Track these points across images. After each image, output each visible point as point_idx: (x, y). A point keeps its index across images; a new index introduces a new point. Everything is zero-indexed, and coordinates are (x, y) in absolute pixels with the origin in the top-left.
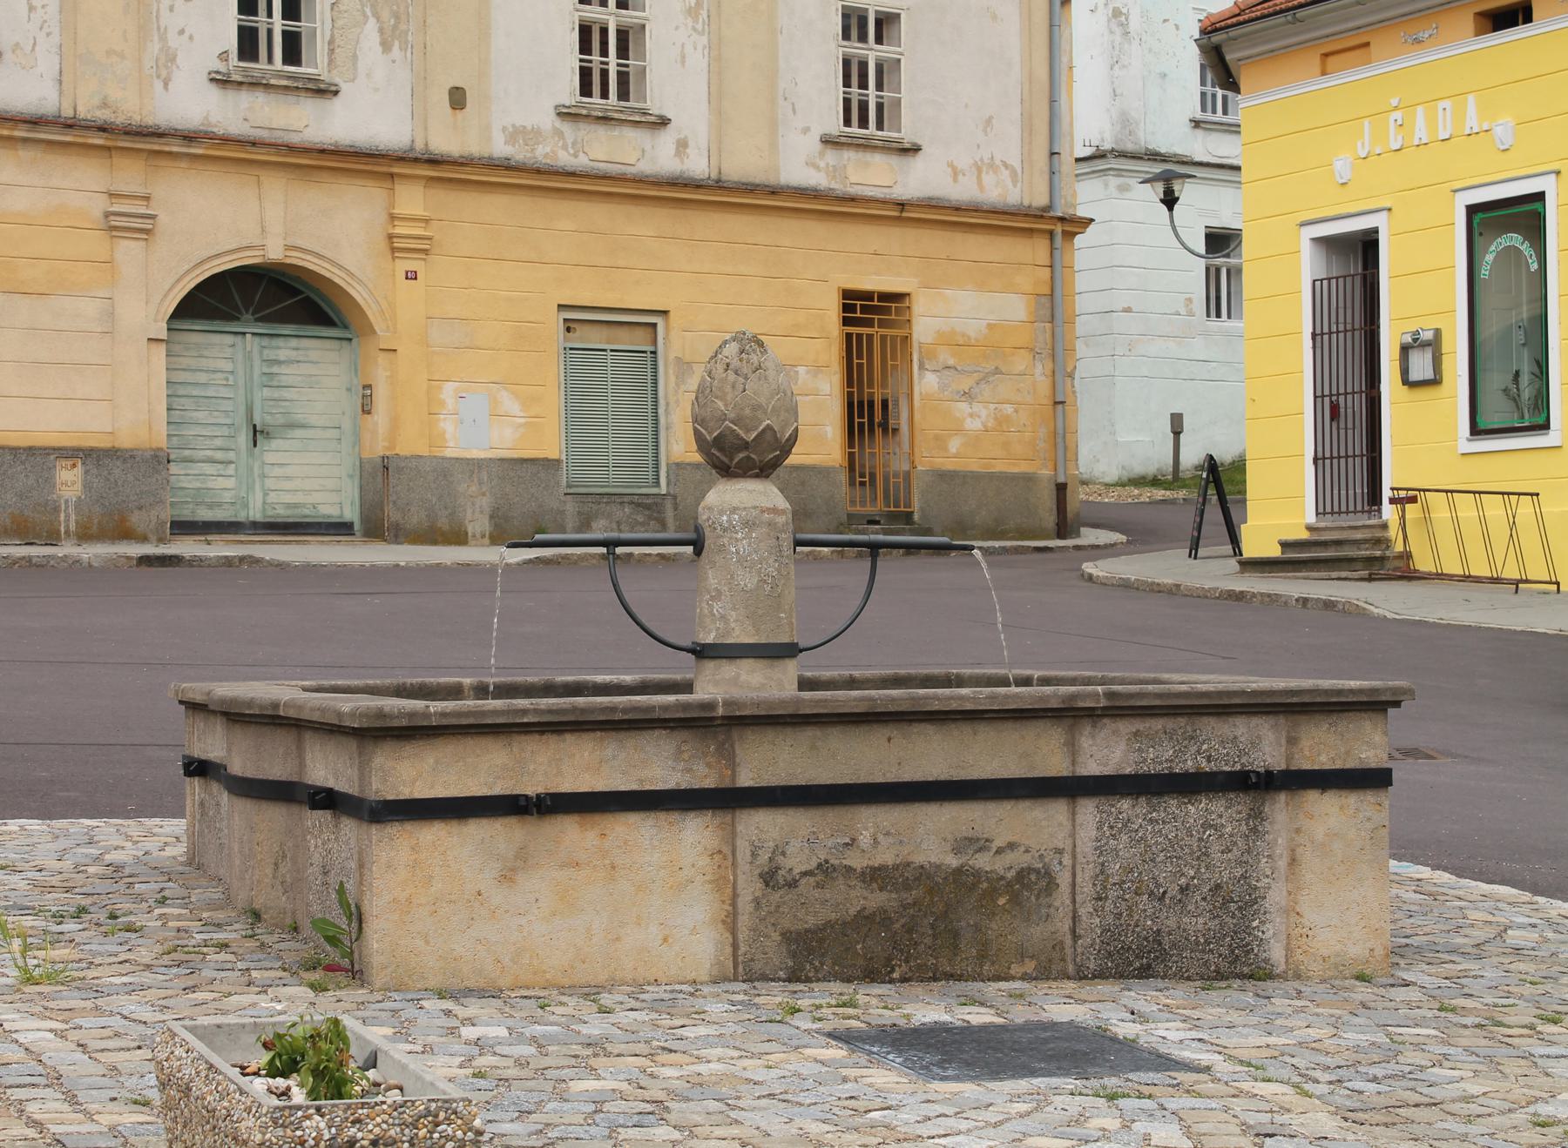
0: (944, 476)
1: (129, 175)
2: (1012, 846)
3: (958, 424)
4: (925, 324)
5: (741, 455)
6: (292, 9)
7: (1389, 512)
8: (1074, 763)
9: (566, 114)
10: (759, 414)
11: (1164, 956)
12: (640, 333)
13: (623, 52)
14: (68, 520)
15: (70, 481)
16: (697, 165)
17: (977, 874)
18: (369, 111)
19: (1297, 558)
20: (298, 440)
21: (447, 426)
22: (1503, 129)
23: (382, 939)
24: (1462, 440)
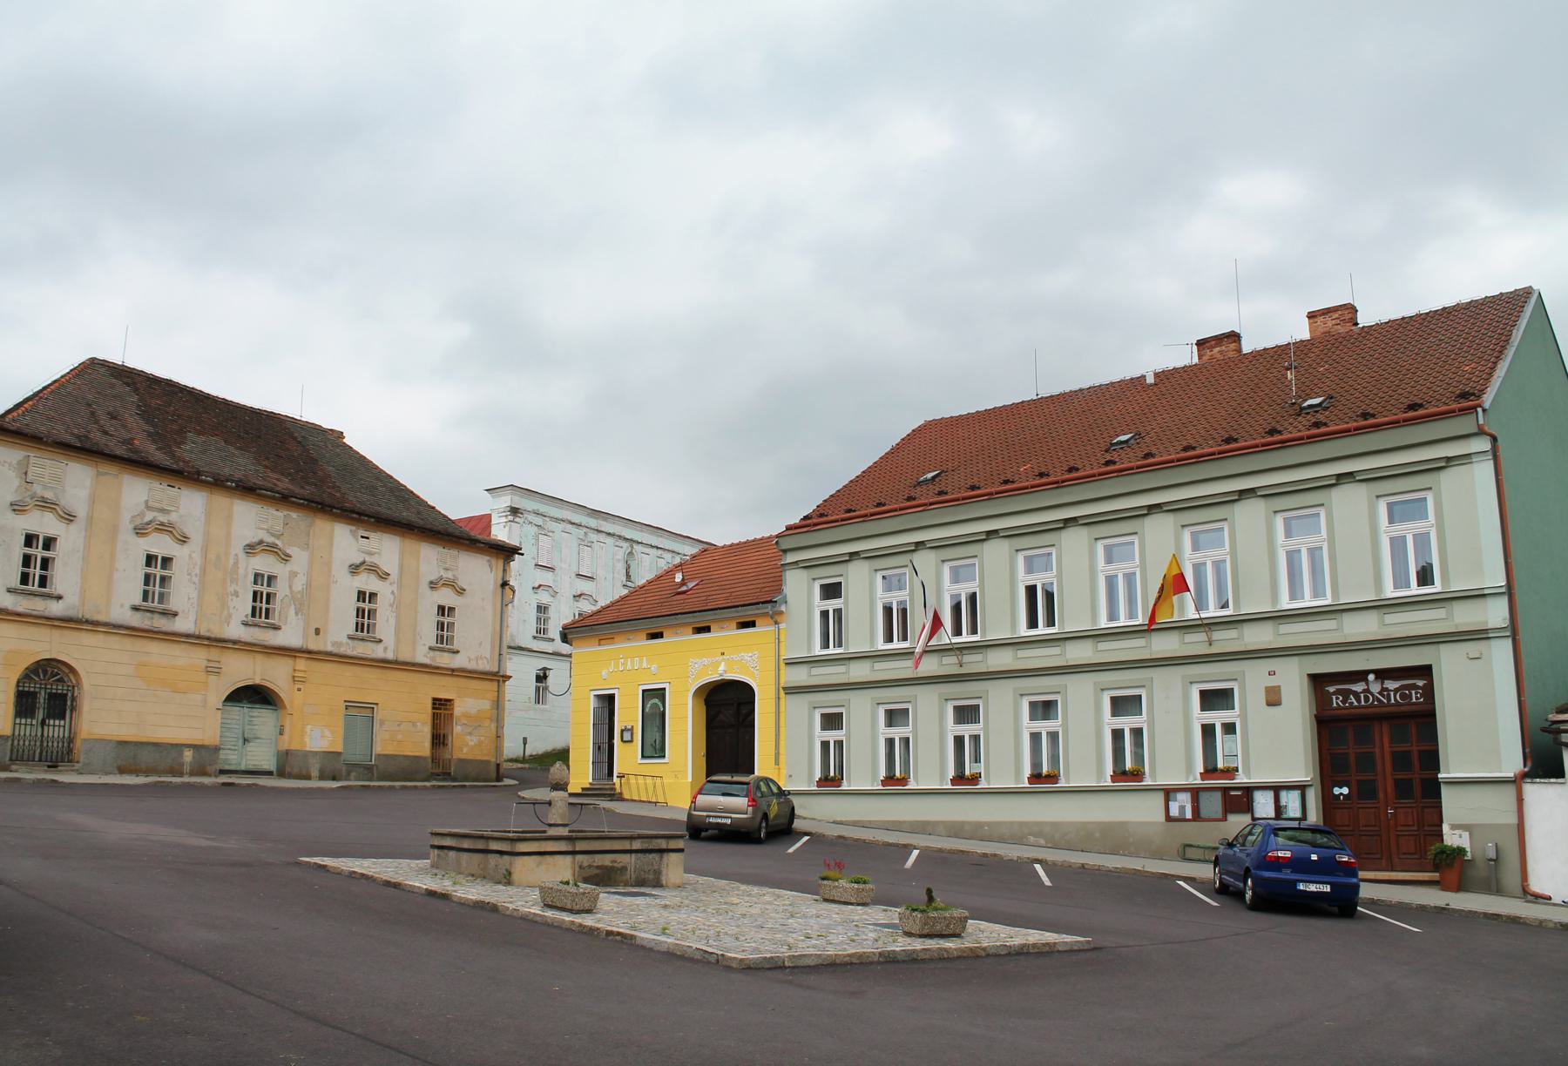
0: (461, 760)
1: (214, 654)
3: (467, 743)
4: (458, 709)
7: (615, 779)
9: (351, 638)
14: (187, 768)
15: (188, 755)
16: (390, 656)
18: (290, 634)
19: (586, 792)
20: (257, 744)
21: (307, 740)
23: (516, 877)
24: (640, 761)
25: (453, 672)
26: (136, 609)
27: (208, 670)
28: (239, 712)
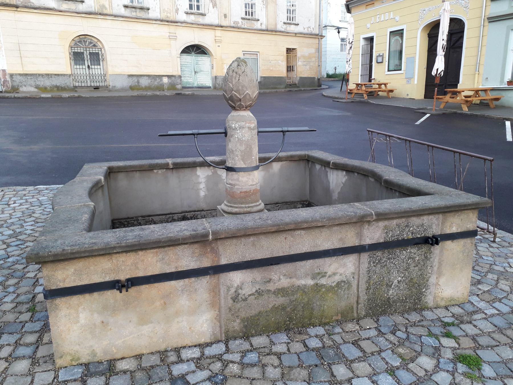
1: (172, 29)
2: (334, 274)
4: (299, 54)
5: (239, 103)
6: (198, 1)
8: (361, 240)
10: (245, 89)
11: (390, 306)
12: (255, 55)
13: (252, 8)
16: (264, 27)
17: (323, 286)
18: (210, 19)
22: (397, 18)
25: (296, 34)
26: (126, 7)
27: (170, 38)
28: (191, 58)
